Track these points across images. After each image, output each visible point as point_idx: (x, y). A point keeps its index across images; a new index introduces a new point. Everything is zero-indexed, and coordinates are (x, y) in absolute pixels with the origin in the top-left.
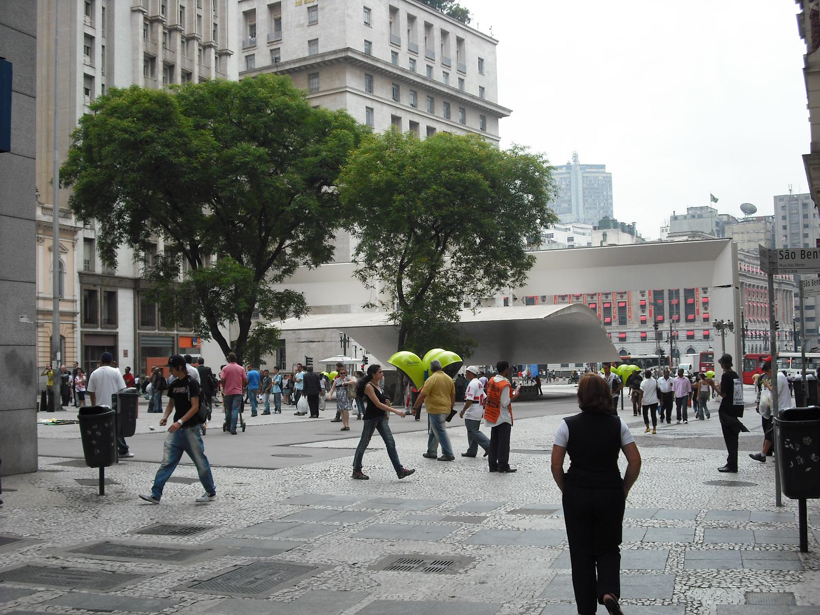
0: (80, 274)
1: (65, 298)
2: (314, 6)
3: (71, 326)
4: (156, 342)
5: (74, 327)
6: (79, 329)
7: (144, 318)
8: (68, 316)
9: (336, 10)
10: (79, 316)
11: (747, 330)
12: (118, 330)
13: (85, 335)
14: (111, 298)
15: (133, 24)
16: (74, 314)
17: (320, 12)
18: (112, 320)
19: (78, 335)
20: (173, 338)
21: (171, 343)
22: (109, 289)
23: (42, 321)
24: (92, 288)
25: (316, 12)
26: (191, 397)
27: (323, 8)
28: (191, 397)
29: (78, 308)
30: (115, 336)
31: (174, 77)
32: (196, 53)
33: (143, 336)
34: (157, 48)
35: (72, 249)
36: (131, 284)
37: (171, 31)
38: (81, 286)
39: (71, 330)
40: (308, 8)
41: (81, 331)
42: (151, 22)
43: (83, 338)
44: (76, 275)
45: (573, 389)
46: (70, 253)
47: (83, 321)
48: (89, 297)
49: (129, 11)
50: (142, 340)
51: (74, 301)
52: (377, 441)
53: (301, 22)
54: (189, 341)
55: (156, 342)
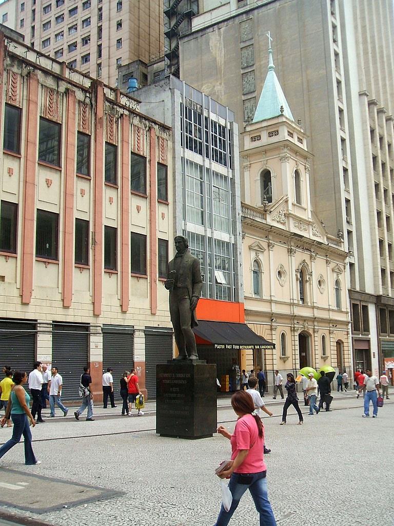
0: (349, 291)
6: (350, 335)
8: (287, 319)
12: (370, 336)
13: (355, 341)
14: (365, 309)
15: (361, 104)
19: (350, 340)
23: (317, 328)
24: (384, 308)
30: (368, 341)
35: (267, 250)
37: (380, 111)
38: (350, 301)
42: (371, 103)
45: (33, 365)
46: (266, 252)
49: (358, 95)
50: (383, 344)
51: (347, 313)
52: (247, 498)
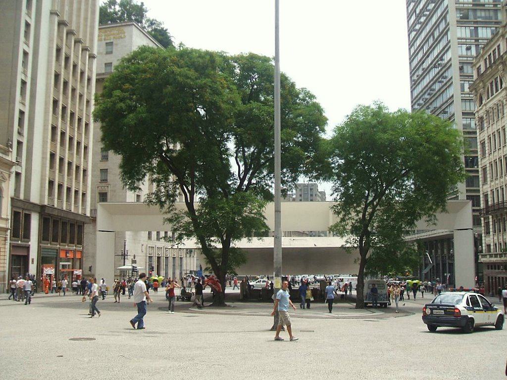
0: (12, 199)
1: (2, 216)
2: (110, 43)
3: (3, 239)
4: (49, 253)
5: (6, 239)
6: (8, 241)
7: (44, 236)
9: (125, 46)
10: (9, 231)
11: (127, 255)
12: (30, 243)
13: (13, 247)
14: (28, 218)
15: (51, 22)
16: (6, 230)
17: (114, 47)
18: (27, 236)
19: (8, 246)
20: (57, 250)
21: (55, 254)
22: (27, 212)
25: (111, 47)
26: (430, 308)
27: (117, 45)
28: (430, 308)
29: (8, 225)
30: (28, 248)
31: (68, 65)
32: (80, 52)
33: (43, 248)
34: (62, 43)
36: (39, 209)
39: (3, 242)
40: (106, 43)
41: (10, 243)
42: (61, 24)
43: (11, 248)
44: (10, 199)
47: (12, 235)
48: (16, 215)
50: (42, 251)
51: (7, 220)
53: (101, 51)
54: (64, 252)
55: (49, 253)
